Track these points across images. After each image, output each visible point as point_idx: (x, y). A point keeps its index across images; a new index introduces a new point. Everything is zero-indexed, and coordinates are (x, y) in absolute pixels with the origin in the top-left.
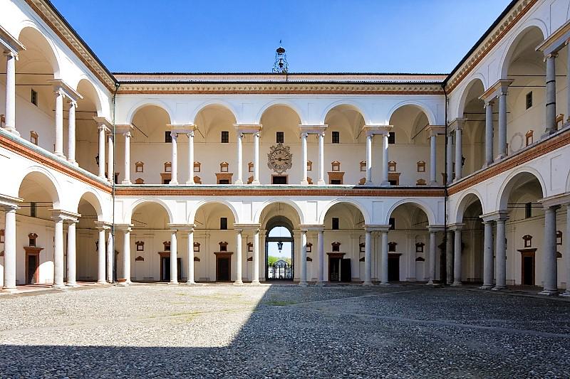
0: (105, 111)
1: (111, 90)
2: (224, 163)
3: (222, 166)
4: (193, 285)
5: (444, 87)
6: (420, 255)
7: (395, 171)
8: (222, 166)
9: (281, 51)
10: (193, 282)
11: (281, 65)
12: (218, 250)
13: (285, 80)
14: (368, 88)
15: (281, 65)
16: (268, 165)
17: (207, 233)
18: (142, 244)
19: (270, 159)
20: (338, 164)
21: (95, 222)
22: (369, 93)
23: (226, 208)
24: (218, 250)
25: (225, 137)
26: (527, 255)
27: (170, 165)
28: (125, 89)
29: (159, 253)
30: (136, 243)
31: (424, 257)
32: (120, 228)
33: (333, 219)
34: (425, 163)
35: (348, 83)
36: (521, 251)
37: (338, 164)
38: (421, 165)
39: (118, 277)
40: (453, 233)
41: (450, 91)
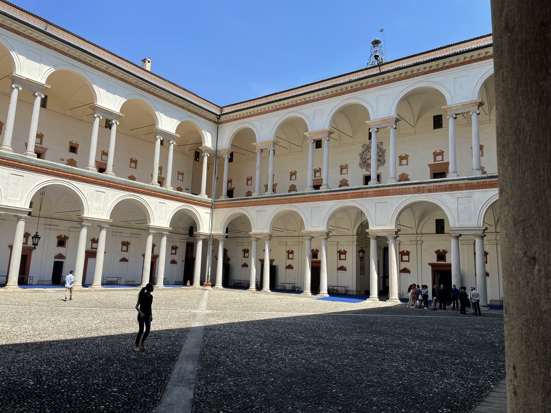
0: (208, 142)
1: (214, 122)
2: (438, 151)
3: (436, 154)
4: (324, 299)
5: (218, 119)
6: (342, 263)
7: (443, 160)
8: (436, 154)
9: (376, 43)
10: (254, 290)
11: (376, 57)
12: (434, 260)
13: (379, 72)
14: (465, 58)
15: (376, 57)
16: (360, 165)
17: (419, 238)
18: (292, 252)
19: (362, 159)
20: (441, 153)
21: (367, 230)
22: (448, 67)
23: (436, 208)
24: (434, 260)
25: (438, 122)
26: (315, 265)
27: (320, 170)
28: (225, 119)
29: (429, 264)
30: (338, 252)
31: (345, 266)
32: (216, 237)
33: (436, 220)
34: (408, 156)
35: (350, 82)
36: (432, 265)
37: (441, 153)
38: (343, 168)
39: (259, 287)
40: (216, 242)
41: (221, 123)
